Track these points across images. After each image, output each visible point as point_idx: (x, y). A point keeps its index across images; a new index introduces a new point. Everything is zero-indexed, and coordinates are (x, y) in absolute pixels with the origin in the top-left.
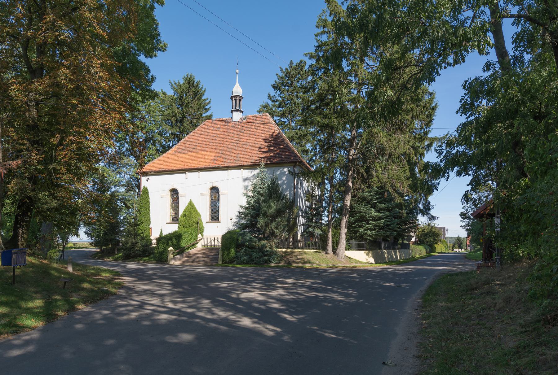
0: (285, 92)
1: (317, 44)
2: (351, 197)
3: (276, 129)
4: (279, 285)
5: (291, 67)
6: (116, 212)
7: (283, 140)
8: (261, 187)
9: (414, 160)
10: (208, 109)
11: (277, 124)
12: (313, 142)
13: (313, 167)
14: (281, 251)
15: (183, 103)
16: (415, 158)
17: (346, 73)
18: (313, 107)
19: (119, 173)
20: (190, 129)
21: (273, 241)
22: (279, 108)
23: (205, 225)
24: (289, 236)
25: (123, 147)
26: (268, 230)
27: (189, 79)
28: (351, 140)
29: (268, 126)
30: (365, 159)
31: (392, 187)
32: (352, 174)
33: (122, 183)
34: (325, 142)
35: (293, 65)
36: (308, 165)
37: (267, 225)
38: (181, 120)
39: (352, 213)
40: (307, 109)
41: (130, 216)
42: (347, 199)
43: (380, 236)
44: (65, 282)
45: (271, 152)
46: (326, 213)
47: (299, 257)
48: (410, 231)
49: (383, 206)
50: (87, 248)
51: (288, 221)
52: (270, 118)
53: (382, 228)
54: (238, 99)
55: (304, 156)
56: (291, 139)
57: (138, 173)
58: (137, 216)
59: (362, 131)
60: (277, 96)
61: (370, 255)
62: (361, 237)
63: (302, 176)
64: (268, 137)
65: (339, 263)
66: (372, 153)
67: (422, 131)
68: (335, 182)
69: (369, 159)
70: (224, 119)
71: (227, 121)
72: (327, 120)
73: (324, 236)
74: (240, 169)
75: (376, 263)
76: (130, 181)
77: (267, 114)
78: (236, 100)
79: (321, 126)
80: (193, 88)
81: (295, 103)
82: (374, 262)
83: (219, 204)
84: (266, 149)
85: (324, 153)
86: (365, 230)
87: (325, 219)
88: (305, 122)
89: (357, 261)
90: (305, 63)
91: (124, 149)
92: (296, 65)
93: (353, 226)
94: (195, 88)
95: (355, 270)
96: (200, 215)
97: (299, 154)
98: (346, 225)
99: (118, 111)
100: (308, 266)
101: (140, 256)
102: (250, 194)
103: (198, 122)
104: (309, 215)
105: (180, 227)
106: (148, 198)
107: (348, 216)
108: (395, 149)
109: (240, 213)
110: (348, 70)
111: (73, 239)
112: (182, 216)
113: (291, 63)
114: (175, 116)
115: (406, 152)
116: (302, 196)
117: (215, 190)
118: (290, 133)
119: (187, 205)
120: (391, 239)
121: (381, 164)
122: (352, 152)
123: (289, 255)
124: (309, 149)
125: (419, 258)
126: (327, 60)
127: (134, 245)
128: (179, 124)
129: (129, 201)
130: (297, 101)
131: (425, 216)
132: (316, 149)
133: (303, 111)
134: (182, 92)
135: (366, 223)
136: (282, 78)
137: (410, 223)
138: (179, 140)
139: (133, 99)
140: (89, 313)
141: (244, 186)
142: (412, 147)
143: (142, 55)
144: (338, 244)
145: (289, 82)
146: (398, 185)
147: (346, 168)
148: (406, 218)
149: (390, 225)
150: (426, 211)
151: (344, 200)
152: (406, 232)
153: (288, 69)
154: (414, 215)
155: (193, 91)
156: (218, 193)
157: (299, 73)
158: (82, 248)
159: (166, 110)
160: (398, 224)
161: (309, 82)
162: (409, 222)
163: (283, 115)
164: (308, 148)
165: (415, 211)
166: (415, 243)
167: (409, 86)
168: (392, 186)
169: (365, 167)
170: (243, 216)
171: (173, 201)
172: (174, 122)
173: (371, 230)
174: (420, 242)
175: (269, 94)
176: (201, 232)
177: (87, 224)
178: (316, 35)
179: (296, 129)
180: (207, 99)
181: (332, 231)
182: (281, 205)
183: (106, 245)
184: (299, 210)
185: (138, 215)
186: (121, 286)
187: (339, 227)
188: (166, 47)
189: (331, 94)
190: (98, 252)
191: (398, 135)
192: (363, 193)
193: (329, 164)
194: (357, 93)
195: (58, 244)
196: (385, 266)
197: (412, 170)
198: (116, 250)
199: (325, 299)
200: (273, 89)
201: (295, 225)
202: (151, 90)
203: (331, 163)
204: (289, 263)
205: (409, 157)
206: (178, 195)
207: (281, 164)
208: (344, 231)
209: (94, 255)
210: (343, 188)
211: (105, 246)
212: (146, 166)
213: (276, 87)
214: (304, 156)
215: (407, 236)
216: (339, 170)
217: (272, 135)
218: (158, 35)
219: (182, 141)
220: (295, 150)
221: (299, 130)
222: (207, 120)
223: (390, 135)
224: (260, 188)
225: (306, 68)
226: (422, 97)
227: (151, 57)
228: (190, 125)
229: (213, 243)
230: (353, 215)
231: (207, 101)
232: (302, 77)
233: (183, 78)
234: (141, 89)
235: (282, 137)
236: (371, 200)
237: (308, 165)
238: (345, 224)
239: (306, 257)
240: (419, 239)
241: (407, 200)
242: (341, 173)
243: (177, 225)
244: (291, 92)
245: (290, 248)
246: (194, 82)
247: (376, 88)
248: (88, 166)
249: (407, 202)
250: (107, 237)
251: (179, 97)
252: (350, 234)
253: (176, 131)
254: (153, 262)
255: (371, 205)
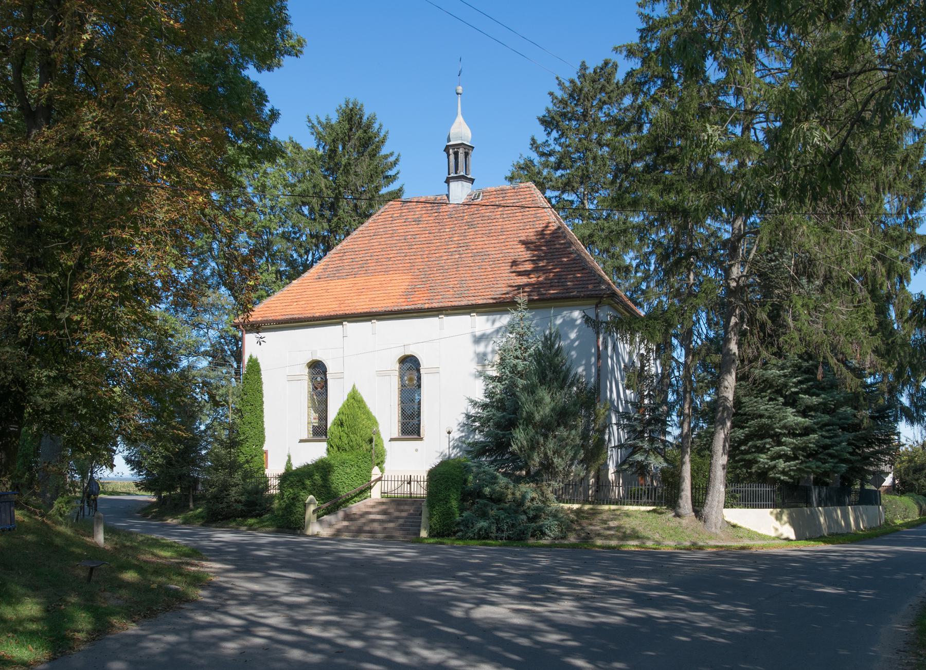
0: (570, 134)
1: (644, 26)
2: (738, 379)
3: (553, 218)
4: (562, 589)
5: (584, 76)
6: (190, 415)
7: (570, 244)
8: (520, 356)
9: (885, 288)
10: (392, 179)
11: (553, 206)
12: (641, 248)
13: (641, 306)
14: (569, 509)
15: (336, 164)
16: (887, 284)
17: (713, 85)
18: (639, 165)
19: (197, 326)
20: (353, 223)
21: (549, 485)
22: (556, 169)
23: (387, 445)
24: (588, 472)
25: (205, 268)
26: (536, 459)
27: (351, 110)
28: (733, 243)
29: (532, 211)
30: (767, 288)
31: (836, 355)
32: (736, 324)
33: (203, 349)
34: (669, 247)
35: (588, 72)
36: (629, 303)
37: (533, 446)
38: (332, 204)
39: (740, 417)
40: (625, 171)
41: (220, 424)
42: (726, 383)
43: (808, 473)
44: (92, 569)
45: (541, 274)
46: (675, 417)
47: (612, 524)
48: (880, 460)
49: (815, 400)
50: (129, 494)
51: (585, 436)
52: (537, 193)
53: (812, 455)
54: (461, 151)
55: (619, 281)
56: (589, 241)
57: (236, 326)
58: (234, 423)
59: (758, 221)
60: (551, 142)
61: (785, 518)
62: (763, 476)
63: (617, 329)
64: (533, 238)
65: (710, 538)
66: (783, 273)
67: (901, 221)
68: (697, 342)
69: (777, 288)
70: (431, 197)
71: (436, 204)
72: (672, 195)
73: (673, 473)
74: (469, 314)
75: (799, 537)
76: (220, 343)
77: (531, 184)
78: (456, 154)
79: (660, 211)
80: (361, 131)
81: (594, 158)
82: (793, 537)
83: (420, 395)
84: (528, 266)
85: (668, 272)
86: (772, 458)
87: (674, 432)
88: (619, 202)
89: (752, 535)
90: (615, 66)
91: (208, 272)
92: (595, 72)
93: (743, 448)
94: (365, 132)
95: (745, 556)
96: (375, 422)
97: (607, 277)
98: (724, 446)
99: (199, 189)
100: (632, 545)
101: (245, 515)
102: (494, 372)
103: (371, 206)
104: (635, 423)
105: (331, 449)
106: (259, 381)
107: (729, 424)
108: (839, 264)
109: (468, 416)
110: (718, 81)
111: (103, 474)
112: (334, 424)
113: (584, 67)
114: (319, 195)
115: (865, 270)
116: (618, 374)
117: (410, 364)
118: (585, 226)
119: (346, 398)
120: (834, 480)
121: (806, 300)
122: (736, 271)
123: (587, 518)
124: (630, 265)
125: (901, 525)
126: (666, 56)
127: (225, 487)
128: (327, 213)
129: (217, 388)
130: (600, 153)
131: (916, 424)
132: (649, 264)
133: (616, 177)
134: (334, 141)
135: (774, 441)
136: (562, 101)
137: (881, 442)
138: (328, 248)
139: (232, 162)
140: (139, 638)
141: (478, 355)
142: (878, 257)
143: (251, 67)
144: (706, 494)
145: (580, 110)
146: (849, 350)
147: (722, 308)
148: (869, 429)
149: (832, 446)
150: (917, 411)
151: (720, 386)
152: (871, 464)
153: (577, 81)
154: (890, 422)
155: (360, 139)
156: (418, 371)
157: (603, 89)
158: (118, 494)
159: (299, 181)
160: (849, 444)
161: (626, 110)
162: (878, 440)
163: (567, 186)
164: (628, 261)
165: (890, 413)
166: (893, 489)
167: (867, 115)
168: (834, 348)
169: (768, 308)
170: (477, 424)
171: (315, 388)
172: (317, 208)
173: (787, 458)
174: (903, 488)
175: (533, 139)
176: (379, 461)
177: (130, 441)
178: (640, 5)
179: (599, 219)
180: (392, 154)
181: (691, 461)
182: (562, 398)
183: (171, 488)
184: (609, 409)
185: (238, 421)
186: (198, 581)
187: (707, 452)
188: (302, 47)
189: (680, 137)
190: (152, 505)
191: (845, 228)
192: (766, 369)
193: (680, 301)
194: (743, 132)
195: (73, 484)
196: (822, 546)
197: (882, 311)
198: (191, 500)
199: (674, 627)
200: (543, 128)
201: (601, 445)
202: (267, 141)
203: (685, 296)
204: (587, 538)
205: (874, 281)
206: (325, 375)
207: (565, 300)
208: (721, 460)
209: (144, 510)
210: (717, 358)
211: (168, 489)
212: (256, 308)
213: (548, 122)
214: (619, 281)
215: (874, 473)
216: (704, 314)
217: (541, 234)
218: (285, 21)
219: (334, 251)
220: (599, 267)
221: (606, 219)
222: (391, 203)
223: (827, 231)
224: (517, 358)
225: (620, 76)
226: (898, 139)
227: (270, 69)
228: (353, 214)
229: (406, 489)
230: (743, 422)
231: (392, 159)
232: (609, 98)
233: (337, 111)
234: (246, 140)
235: (565, 237)
236: (785, 385)
237: (629, 303)
238: (721, 443)
239: (628, 524)
240: (901, 480)
241: (872, 385)
242: (709, 322)
243: (324, 445)
244: (585, 133)
245: (590, 503)
246: (361, 118)
247: (787, 125)
248: (135, 313)
249: (872, 391)
250: (172, 471)
251: (329, 153)
252: (735, 468)
253: (322, 228)
254: (268, 529)
255: (785, 397)
